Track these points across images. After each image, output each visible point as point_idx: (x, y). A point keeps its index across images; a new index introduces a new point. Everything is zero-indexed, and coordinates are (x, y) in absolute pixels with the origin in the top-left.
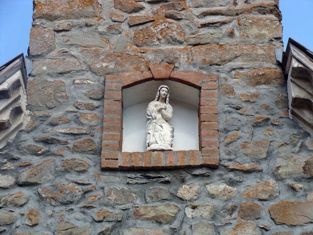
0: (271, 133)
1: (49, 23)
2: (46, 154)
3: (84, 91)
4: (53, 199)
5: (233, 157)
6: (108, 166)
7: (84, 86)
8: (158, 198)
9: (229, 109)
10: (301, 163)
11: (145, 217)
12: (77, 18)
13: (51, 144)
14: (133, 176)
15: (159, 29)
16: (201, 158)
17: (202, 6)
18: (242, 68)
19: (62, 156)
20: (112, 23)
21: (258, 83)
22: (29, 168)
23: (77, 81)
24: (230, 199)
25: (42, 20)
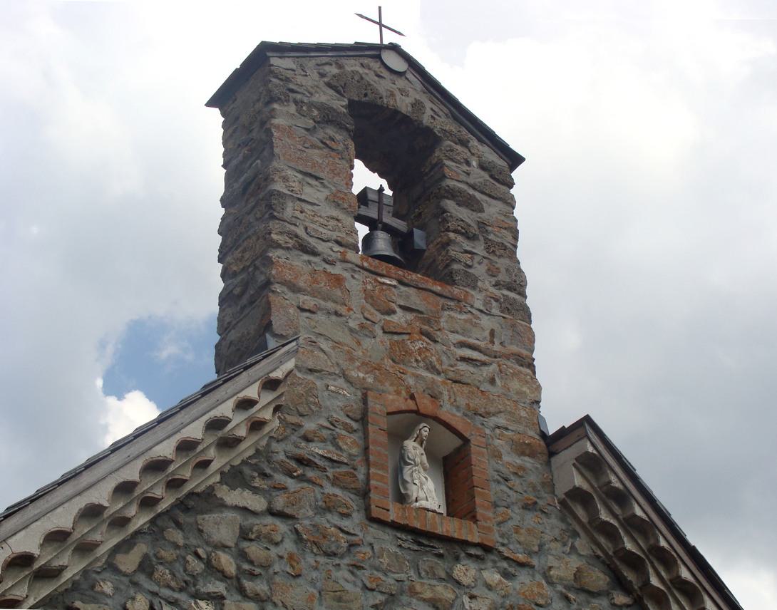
0: (541, 522)
1: (290, 295)
2: (300, 478)
3: (339, 403)
4: (316, 544)
5: (506, 541)
6: (379, 517)
7: (340, 397)
8: (434, 574)
9: (499, 478)
10: (573, 567)
11: (421, 596)
12: (324, 299)
13: (307, 465)
14: (404, 537)
15: (417, 347)
16: (478, 534)
17: (458, 333)
18: (507, 429)
19: (321, 486)
20: (365, 321)
21: (523, 454)
22: (285, 493)
23: (332, 388)
24: (508, 596)
25: (283, 287)
